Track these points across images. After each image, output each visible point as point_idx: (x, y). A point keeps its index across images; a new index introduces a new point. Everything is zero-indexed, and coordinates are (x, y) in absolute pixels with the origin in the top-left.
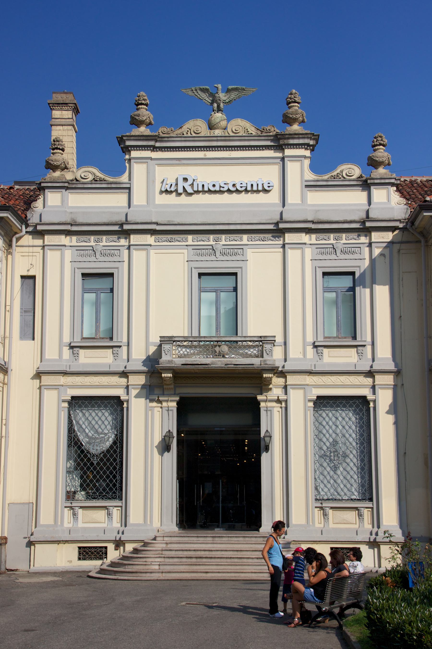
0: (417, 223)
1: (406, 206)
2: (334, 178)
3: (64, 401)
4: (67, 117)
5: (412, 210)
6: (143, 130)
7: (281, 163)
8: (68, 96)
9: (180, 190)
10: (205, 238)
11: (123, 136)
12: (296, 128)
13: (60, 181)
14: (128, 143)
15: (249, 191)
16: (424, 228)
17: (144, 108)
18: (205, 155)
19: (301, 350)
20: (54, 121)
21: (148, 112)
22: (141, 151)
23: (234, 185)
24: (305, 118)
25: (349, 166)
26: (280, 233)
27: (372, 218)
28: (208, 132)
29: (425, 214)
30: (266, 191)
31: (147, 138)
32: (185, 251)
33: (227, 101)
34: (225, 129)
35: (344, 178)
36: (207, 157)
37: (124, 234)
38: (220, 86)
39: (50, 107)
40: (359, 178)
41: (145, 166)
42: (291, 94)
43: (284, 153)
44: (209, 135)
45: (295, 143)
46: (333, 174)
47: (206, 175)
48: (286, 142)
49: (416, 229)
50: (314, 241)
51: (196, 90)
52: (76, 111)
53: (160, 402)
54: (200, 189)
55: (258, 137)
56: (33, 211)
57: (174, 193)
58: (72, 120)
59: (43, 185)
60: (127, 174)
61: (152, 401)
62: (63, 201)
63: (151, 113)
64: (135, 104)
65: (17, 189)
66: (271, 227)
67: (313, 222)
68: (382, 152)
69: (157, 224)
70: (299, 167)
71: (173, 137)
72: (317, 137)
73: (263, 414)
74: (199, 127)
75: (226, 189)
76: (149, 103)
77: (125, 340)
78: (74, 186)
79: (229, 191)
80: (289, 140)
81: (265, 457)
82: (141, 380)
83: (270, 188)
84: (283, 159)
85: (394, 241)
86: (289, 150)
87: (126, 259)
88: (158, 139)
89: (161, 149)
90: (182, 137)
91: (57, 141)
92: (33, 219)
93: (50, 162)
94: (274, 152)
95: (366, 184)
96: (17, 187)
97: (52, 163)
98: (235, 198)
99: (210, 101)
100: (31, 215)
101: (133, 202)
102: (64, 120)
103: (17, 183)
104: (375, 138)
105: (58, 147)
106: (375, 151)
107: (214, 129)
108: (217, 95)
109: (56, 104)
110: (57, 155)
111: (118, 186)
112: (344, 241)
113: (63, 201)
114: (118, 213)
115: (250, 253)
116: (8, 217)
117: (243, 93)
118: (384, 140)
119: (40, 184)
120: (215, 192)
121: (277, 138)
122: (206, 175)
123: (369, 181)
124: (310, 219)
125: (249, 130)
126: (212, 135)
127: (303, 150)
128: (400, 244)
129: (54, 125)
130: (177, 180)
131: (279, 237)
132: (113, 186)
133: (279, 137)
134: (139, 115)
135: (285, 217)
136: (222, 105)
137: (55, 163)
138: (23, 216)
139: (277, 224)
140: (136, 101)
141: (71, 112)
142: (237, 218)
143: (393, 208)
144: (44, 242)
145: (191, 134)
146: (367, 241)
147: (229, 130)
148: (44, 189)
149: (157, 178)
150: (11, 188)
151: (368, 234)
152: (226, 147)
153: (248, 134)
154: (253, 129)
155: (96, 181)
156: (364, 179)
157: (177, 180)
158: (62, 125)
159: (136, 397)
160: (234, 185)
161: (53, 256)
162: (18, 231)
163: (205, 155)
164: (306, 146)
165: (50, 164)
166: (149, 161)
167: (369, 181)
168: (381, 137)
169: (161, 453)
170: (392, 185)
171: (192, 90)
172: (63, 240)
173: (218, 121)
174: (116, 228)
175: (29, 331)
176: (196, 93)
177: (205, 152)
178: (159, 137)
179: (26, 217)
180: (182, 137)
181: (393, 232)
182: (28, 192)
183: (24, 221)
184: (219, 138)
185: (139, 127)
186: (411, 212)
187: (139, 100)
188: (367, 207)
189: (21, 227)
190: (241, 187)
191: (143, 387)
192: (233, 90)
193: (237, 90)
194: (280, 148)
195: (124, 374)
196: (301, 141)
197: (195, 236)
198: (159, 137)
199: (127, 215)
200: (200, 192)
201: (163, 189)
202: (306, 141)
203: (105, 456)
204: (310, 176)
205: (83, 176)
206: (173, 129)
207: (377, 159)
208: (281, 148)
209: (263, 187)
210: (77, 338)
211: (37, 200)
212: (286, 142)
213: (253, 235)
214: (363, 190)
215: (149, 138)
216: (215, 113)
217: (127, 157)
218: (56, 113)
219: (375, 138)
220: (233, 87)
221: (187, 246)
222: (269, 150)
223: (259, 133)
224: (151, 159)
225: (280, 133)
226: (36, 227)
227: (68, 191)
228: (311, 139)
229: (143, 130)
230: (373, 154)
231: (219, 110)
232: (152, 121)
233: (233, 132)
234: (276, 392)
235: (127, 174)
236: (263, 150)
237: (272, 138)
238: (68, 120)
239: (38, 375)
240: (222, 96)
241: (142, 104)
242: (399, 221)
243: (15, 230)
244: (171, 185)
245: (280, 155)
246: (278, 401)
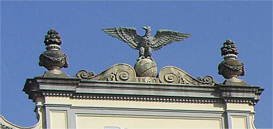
11: (36, 78)
12: (236, 80)
28: (137, 80)
41: (63, 115)
51: (120, 31)
80: (232, 93)
84: (225, 114)
117: (175, 39)
121: (218, 89)
127: (68, 98)
145: (116, 80)
152: (140, 96)
164: (251, 102)
171: (116, 31)
193: (169, 34)
194: (221, 101)
196: (246, 95)
208: (40, 95)
224: (70, 106)
233: (166, 81)
237: (213, 90)
241: (55, 43)
245: (222, 109)
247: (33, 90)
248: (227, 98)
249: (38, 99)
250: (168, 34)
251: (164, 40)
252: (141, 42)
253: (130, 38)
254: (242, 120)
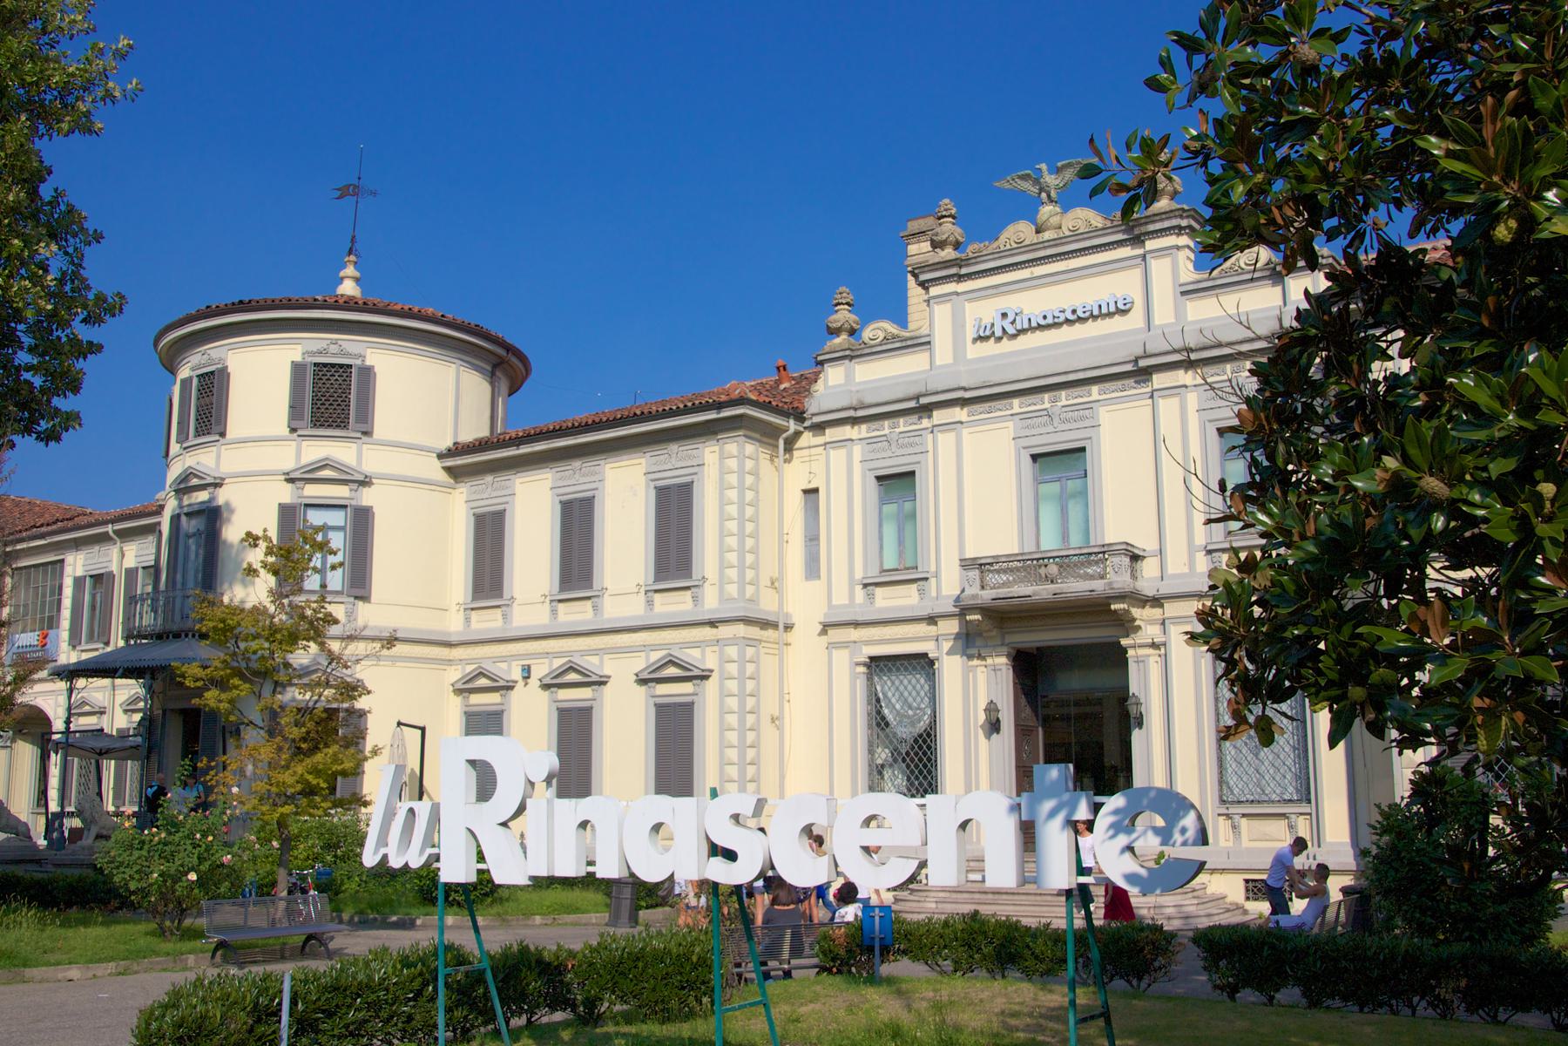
3: (858, 664)
9: (998, 333)
19: (1185, 559)
23: (1074, 312)
30: (1124, 312)
32: (1010, 424)
38: (1044, 166)
47: (1034, 303)
48: (1143, 229)
53: (980, 657)
61: (970, 657)
62: (849, 376)
69: (965, 389)
70: (1172, 260)
73: (1132, 667)
75: (1062, 319)
77: (933, 569)
79: (1067, 321)
81: (1137, 736)
82: (952, 626)
87: (930, 448)
89: (969, 276)
90: (1000, 254)
98: (1079, 331)
115: (1105, 415)
120: (1048, 327)
122: (1034, 303)
136: (1053, 194)
147: (1064, 228)
154: (1099, 219)
159: (948, 653)
160: (1074, 312)
161: (1168, 408)
164: (1179, 230)
169: (988, 737)
172: (847, 431)
175: (812, 568)
180: (1000, 254)
183: (800, 416)
191: (957, 637)
192: (1064, 167)
195: (932, 620)
196: (1166, 224)
197: (1023, 399)
202: (1175, 222)
203: (916, 741)
210: (876, 572)
212: (1143, 229)
213: (1107, 385)
214: (1274, 284)
224: (957, 294)
228: (1181, 217)
234: (1150, 632)
239: (826, 627)
246: (1154, 645)
254: (1175, 401)
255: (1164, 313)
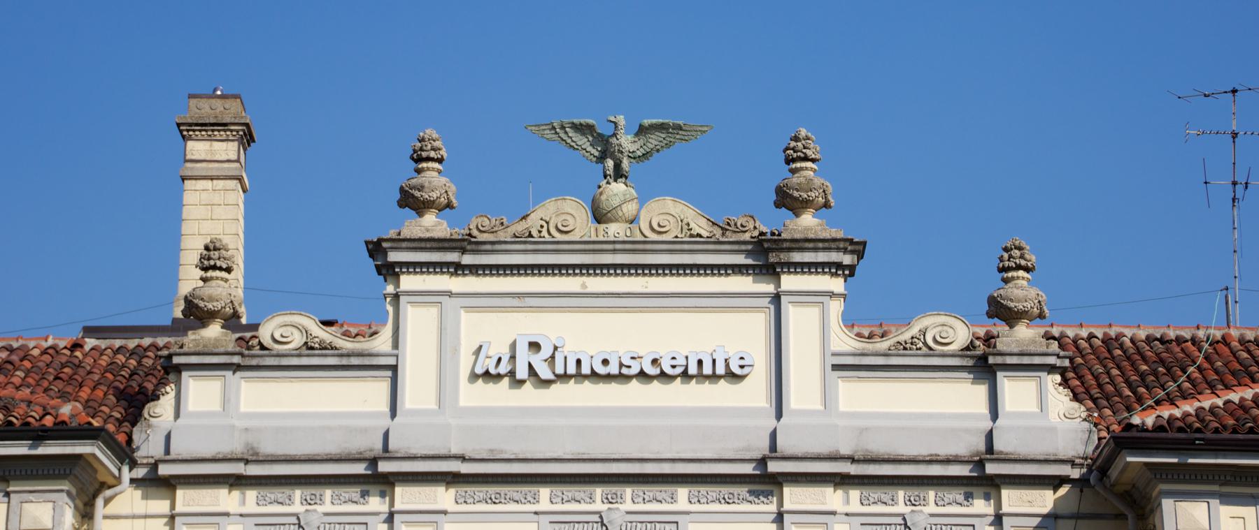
0: (1114, 473)
1: (1086, 425)
2: (905, 349)
4: (224, 157)
5: (1104, 434)
6: (431, 224)
7: (772, 307)
8: (229, 103)
9: (522, 373)
10: (582, 495)
11: (380, 241)
12: (808, 222)
13: (222, 350)
14: (394, 257)
15: (692, 377)
16: (1134, 486)
17: (433, 169)
18: (584, 286)
20: (192, 169)
21: (443, 180)
22: (425, 276)
24: (830, 198)
25: (942, 319)
26: (769, 483)
27: (1001, 453)
28: (593, 230)
29: (1129, 459)
30: (732, 376)
31: (441, 245)
33: (639, 153)
34: (631, 222)
35: (930, 349)
36: (589, 290)
37: (379, 483)
39: (181, 131)
40: (967, 349)
41: (434, 311)
42: (796, 139)
43: (778, 285)
44: (594, 238)
45: (806, 260)
46: (901, 338)
48: (784, 257)
49: (1113, 486)
50: (855, 507)
51: (563, 128)
52: (247, 138)
54: (572, 370)
55: (713, 244)
56: (149, 426)
57: (506, 380)
58: (237, 165)
59: (176, 360)
60: (386, 333)
62: (226, 400)
63: (452, 181)
64: (412, 158)
65: (92, 349)
66: (748, 469)
67: (853, 460)
68: (1022, 288)
69: (463, 458)
71: (506, 242)
72: (861, 248)
74: (569, 217)
75: (635, 370)
76: (445, 155)
78: (254, 362)
79: (642, 375)
83: (745, 371)
84: (776, 298)
85: (1060, 512)
86: (792, 276)
88: (469, 247)
89: (475, 270)
90: (525, 239)
91: (215, 249)
92: (148, 444)
93: (196, 301)
94: (754, 282)
95: (983, 364)
96: (90, 343)
97: (202, 304)
99: (597, 154)
100: (144, 436)
101: (403, 403)
102: (216, 165)
103: (90, 331)
104: (1006, 250)
105: (219, 264)
106: (1006, 281)
107: (605, 222)
108: (614, 140)
109: (197, 125)
110: (214, 283)
111: (367, 361)
112: (932, 508)
113: (225, 401)
114: (364, 431)
116: (94, 455)
118: (1027, 256)
119: (170, 357)
120: (609, 377)
123: (991, 360)
124: (845, 451)
125: (692, 225)
126: (601, 238)
127: (827, 277)
128: (1072, 522)
129: (191, 178)
130: (513, 346)
131: (767, 494)
132: (355, 361)
133: (766, 245)
134: (423, 187)
135: (783, 444)
136: (626, 164)
137: (210, 306)
138: (121, 438)
139: (762, 462)
140: (415, 151)
141: (236, 144)
142: (662, 447)
143: (1053, 430)
144: (173, 506)
146: (990, 510)
148: (178, 369)
149: (463, 342)
150: (76, 346)
151: (993, 492)
153: (692, 236)
154: (703, 222)
155: (312, 348)
156: (979, 352)
157: (513, 346)
158: (212, 178)
160: (655, 362)
162: (110, 481)
163: (584, 286)
164: (835, 268)
165: (197, 306)
166: (444, 299)
167: (991, 360)
168: (1020, 248)
170: (1051, 369)
171: (554, 128)
173: (615, 202)
174: (360, 469)
176: (563, 135)
177: (584, 279)
178: (470, 243)
179: (130, 441)
180: (525, 239)
181: (1055, 489)
182: (121, 358)
183: (125, 454)
184: (618, 246)
185: (420, 214)
186: (1100, 439)
187: (421, 149)
188: (989, 424)
189: (120, 470)
190: (674, 367)
194: (770, 271)
196: (822, 257)
198: (470, 243)
199: (386, 435)
200: (571, 377)
201: (479, 371)
202: (834, 257)
204: (844, 342)
205: (277, 337)
206: (505, 221)
207: (1012, 305)
209: (727, 365)
211: (158, 398)
212: (784, 257)
213: (703, 489)
214: (976, 380)
215: (446, 245)
216: (608, 183)
217: (390, 289)
218: (197, 148)
219: (1006, 250)
220: (654, 121)
221: (536, 513)
222: (743, 274)
223: (718, 232)
224: (450, 294)
225: (769, 236)
226: (155, 466)
227: (238, 374)
228: (845, 251)
229: (431, 224)
230: (1001, 292)
231: (619, 174)
232: (454, 201)
233: (652, 229)
235: (386, 333)
236: (728, 275)
237: (750, 247)
238: (226, 165)
240: (627, 142)
241: (429, 159)
242: (1072, 463)
243: (102, 477)
244: (500, 359)
245: (770, 288)
247: (382, 258)
248: (782, 265)
249: (389, 279)
250: (662, 127)
251: (654, 140)
252: (606, 148)
253: (582, 141)
254: (813, 313)
255: (803, 389)
